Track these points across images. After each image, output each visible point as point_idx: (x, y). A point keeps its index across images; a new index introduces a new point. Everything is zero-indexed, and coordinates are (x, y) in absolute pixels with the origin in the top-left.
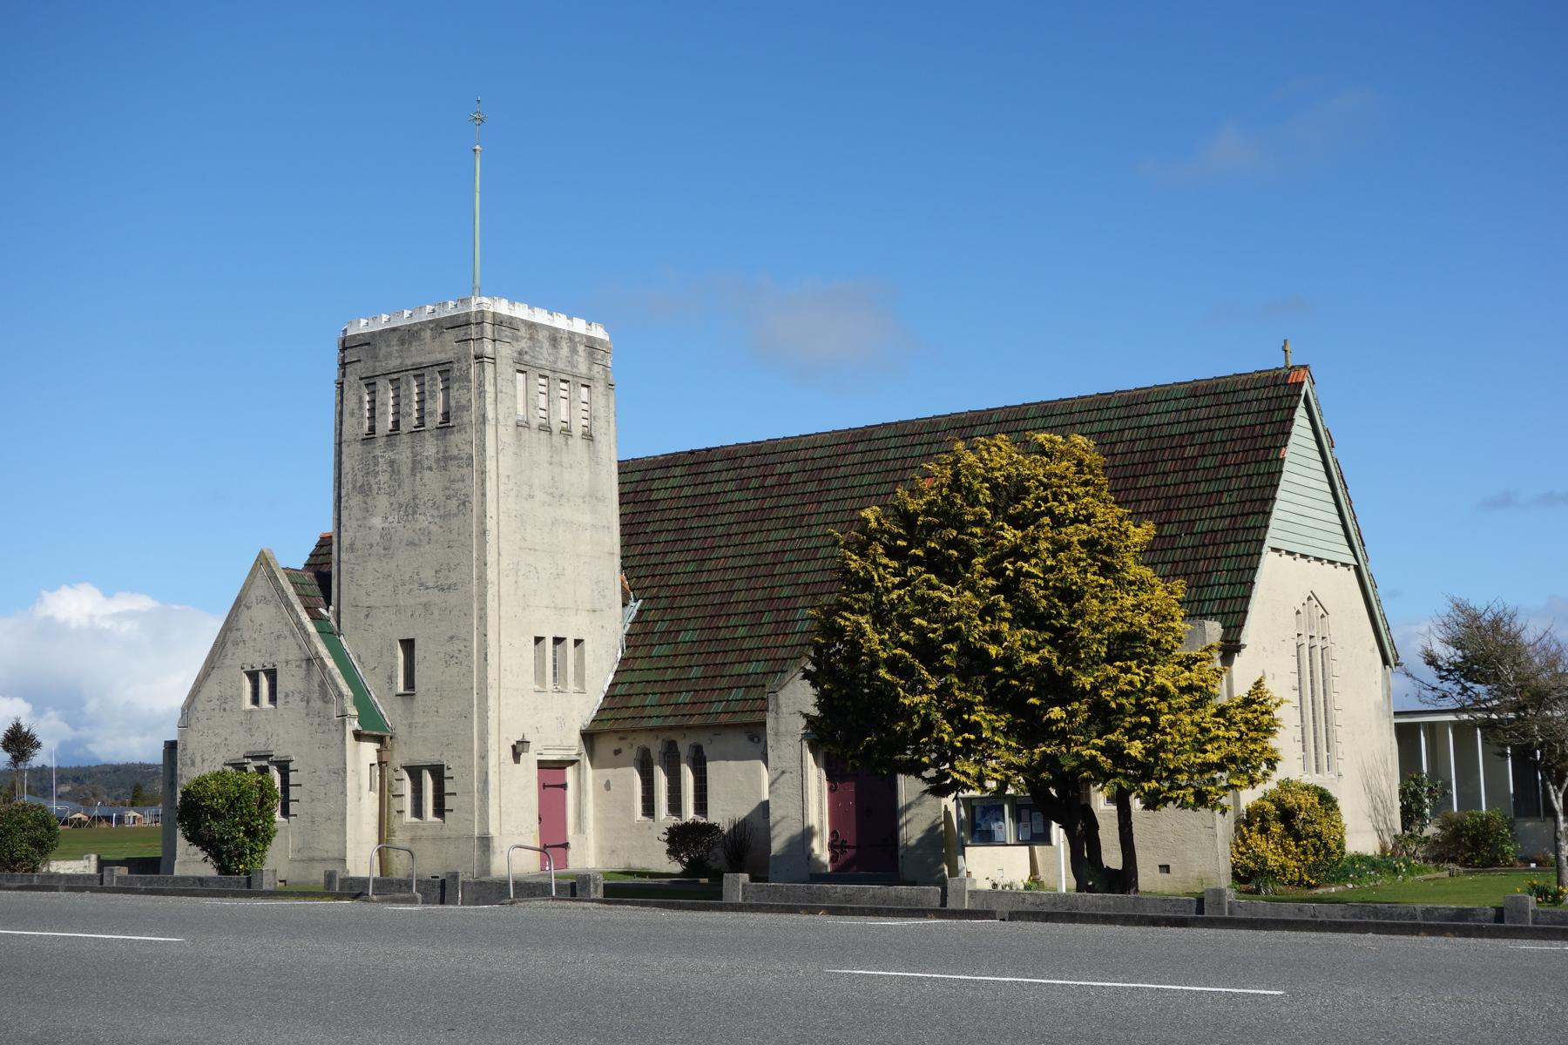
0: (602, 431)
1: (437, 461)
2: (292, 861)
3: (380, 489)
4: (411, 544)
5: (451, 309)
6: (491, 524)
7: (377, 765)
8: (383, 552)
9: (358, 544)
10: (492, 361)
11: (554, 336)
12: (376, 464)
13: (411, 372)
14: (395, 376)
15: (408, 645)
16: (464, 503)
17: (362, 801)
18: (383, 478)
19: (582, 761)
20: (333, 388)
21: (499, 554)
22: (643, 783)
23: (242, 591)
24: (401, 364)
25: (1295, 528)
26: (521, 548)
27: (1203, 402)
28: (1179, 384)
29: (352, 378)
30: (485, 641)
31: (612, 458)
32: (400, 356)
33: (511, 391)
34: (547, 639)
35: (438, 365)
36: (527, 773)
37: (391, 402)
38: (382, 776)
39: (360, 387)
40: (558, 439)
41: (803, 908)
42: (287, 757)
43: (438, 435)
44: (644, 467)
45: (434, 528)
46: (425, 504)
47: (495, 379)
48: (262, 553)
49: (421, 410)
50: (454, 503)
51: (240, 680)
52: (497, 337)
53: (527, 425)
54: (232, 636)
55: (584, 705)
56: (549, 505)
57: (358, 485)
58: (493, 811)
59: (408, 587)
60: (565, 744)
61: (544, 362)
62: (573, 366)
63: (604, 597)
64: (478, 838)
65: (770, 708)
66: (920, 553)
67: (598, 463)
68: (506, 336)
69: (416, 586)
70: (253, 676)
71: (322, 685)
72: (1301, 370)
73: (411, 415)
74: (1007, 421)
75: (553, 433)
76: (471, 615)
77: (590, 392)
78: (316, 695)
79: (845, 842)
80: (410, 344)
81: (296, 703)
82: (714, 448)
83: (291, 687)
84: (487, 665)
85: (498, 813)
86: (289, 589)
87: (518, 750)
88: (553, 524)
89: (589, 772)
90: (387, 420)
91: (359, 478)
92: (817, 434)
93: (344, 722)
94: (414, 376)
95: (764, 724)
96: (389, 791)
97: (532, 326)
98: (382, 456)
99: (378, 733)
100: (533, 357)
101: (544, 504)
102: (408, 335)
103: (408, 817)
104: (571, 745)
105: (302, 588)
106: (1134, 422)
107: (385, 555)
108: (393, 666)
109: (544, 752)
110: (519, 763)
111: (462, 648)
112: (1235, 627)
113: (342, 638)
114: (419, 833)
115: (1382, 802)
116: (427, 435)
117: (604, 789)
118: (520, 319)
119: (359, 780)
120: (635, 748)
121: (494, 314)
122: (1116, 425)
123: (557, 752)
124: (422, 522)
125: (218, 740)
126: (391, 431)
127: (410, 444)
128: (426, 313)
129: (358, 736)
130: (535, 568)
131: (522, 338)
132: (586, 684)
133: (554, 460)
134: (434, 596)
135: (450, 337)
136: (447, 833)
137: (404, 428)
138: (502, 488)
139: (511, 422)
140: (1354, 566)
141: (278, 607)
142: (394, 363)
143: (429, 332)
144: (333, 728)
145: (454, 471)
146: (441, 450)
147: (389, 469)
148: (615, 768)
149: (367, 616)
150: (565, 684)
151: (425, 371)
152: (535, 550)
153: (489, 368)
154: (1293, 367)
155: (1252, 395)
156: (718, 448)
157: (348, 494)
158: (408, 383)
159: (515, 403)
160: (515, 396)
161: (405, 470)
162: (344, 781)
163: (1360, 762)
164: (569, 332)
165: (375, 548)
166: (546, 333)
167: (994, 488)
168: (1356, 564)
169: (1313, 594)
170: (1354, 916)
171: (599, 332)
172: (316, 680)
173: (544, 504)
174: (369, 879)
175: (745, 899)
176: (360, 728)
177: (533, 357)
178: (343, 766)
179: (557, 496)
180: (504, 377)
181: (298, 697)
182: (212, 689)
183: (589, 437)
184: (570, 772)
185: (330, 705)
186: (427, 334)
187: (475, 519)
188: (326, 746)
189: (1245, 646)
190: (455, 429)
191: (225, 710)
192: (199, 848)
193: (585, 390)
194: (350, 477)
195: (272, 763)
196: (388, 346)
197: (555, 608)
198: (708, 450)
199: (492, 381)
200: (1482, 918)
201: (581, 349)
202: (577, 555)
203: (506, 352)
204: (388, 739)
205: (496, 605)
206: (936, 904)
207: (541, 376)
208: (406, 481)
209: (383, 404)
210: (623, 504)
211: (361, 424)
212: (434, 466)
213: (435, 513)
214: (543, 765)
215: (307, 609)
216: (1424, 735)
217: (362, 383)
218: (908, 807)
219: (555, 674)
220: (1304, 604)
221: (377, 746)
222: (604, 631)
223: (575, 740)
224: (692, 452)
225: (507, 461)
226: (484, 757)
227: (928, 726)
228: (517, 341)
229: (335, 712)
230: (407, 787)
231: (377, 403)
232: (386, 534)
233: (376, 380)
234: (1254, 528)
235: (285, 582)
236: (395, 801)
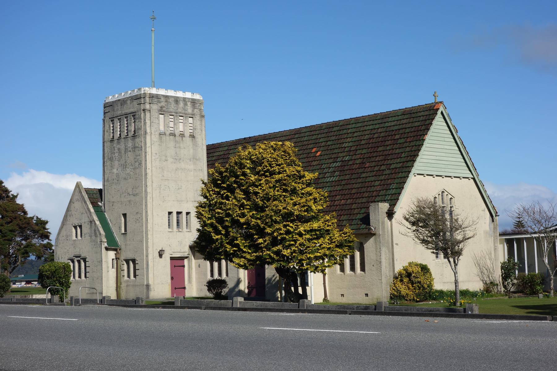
0: (199, 134)
1: (132, 148)
2: (88, 293)
3: (115, 159)
4: (125, 179)
5: (136, 92)
6: (149, 171)
7: (115, 259)
8: (117, 182)
9: (110, 179)
10: (149, 111)
11: (177, 100)
12: (114, 150)
13: (124, 116)
14: (119, 117)
15: (125, 215)
16: (140, 164)
18: (116, 155)
19: (190, 257)
20: (102, 122)
21: (152, 182)
23: (72, 197)
24: (121, 113)
25: (435, 166)
26: (162, 180)
27: (406, 116)
28: (400, 109)
29: (107, 118)
30: (147, 214)
31: (204, 143)
32: (121, 110)
33: (157, 122)
34: (174, 213)
35: (132, 113)
36: (166, 261)
37: (119, 127)
38: (117, 263)
39: (109, 121)
40: (178, 138)
41: (186, 307)
42: (85, 256)
43: (132, 139)
44: (229, 145)
45: (131, 173)
46: (129, 164)
47: (150, 118)
48: (77, 183)
49: (127, 130)
50: (137, 164)
51: (72, 229)
52: (151, 102)
53: (165, 134)
54: (69, 213)
55: (192, 236)
56: (175, 163)
57: (109, 157)
58: (151, 275)
59: (124, 195)
61: (172, 110)
62: (185, 110)
66: (225, 185)
67: (196, 146)
68: (155, 101)
69: (127, 194)
70: (75, 227)
71: (95, 231)
72: (440, 103)
73: (124, 131)
74: (344, 125)
76: (143, 205)
77: (193, 119)
78: (93, 234)
80: (124, 105)
81: (88, 237)
82: (252, 137)
83: (86, 232)
84: (148, 223)
85: (153, 276)
86: (86, 196)
87: (160, 253)
88: (176, 170)
90: (117, 134)
91: (110, 155)
92: (285, 131)
93: (101, 244)
94: (132, 116)
96: (120, 268)
97: (166, 97)
98: (116, 147)
99: (114, 248)
100: (167, 108)
101: (172, 163)
102: (123, 102)
103: (126, 278)
104: (185, 250)
105: (93, 195)
106: (382, 125)
107: (117, 183)
108: (121, 223)
109: (173, 254)
110: (162, 258)
111: (140, 217)
112: (393, 205)
113: (105, 213)
114: (129, 283)
115: (486, 269)
116: (129, 139)
121: (150, 94)
122: (377, 126)
123: (178, 254)
124: (128, 170)
125: (66, 251)
126: (119, 137)
127: (124, 142)
128: (129, 94)
129: (107, 249)
130: (168, 187)
131: (162, 102)
132: (192, 229)
134: (132, 198)
135: (135, 102)
136: (137, 283)
137: (122, 137)
138: (153, 158)
139: (157, 133)
140: (472, 178)
141: (82, 203)
142: (119, 113)
143: (129, 101)
144: (98, 246)
145: (137, 152)
146: (133, 144)
147: (118, 151)
149: (113, 205)
150: (173, 229)
151: (128, 115)
153: (148, 114)
154: (437, 102)
155: (422, 113)
156: (253, 137)
157: (106, 161)
158: (123, 120)
159: (159, 126)
160: (159, 124)
161: (123, 152)
162: (102, 265)
163: (473, 255)
164: (183, 98)
165: (115, 180)
166: (173, 99)
167: (253, 162)
168: (473, 177)
170: (339, 309)
171: (197, 97)
172: (93, 229)
173: (172, 163)
174: (46, 299)
175: (181, 305)
176: (107, 246)
178: (101, 260)
179: (178, 159)
180: (154, 117)
181: (88, 235)
182: (64, 233)
183: (192, 136)
184: (186, 261)
185: (97, 238)
186: (129, 102)
187: (143, 170)
188: (96, 253)
189: (395, 212)
190: (137, 137)
191: (67, 240)
193: (191, 119)
194: (107, 154)
195: (82, 259)
196: (117, 106)
198: (250, 138)
199: (149, 119)
200: (371, 309)
201: (189, 104)
202: (187, 181)
203: (155, 107)
204: (118, 250)
205: (151, 200)
206: (231, 306)
207: (170, 115)
208: (123, 156)
209: (116, 128)
211: (110, 135)
212: (131, 150)
213: (132, 167)
214: (172, 259)
215: (92, 203)
216: (526, 242)
217: (110, 120)
219: (187, 225)
220: (439, 194)
221: (115, 252)
223: (187, 249)
224: (245, 139)
225: (155, 148)
226: (147, 256)
227: (222, 245)
228: (160, 103)
229: (99, 241)
230: (125, 267)
231: (114, 127)
232: (118, 175)
233: (114, 119)
234: (409, 167)
235: (84, 194)
236: (122, 272)
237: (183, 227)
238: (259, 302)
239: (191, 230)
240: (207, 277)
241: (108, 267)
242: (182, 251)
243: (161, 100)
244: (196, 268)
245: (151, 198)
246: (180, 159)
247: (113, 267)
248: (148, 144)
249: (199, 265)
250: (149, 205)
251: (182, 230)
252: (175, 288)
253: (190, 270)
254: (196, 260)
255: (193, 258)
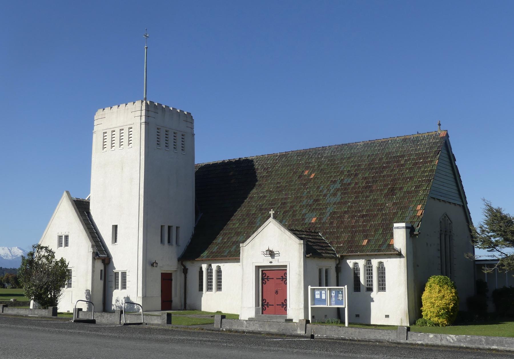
79: (281, 280)
140: (462, 206)
168: (463, 205)
169: (447, 215)
210: (213, 323)
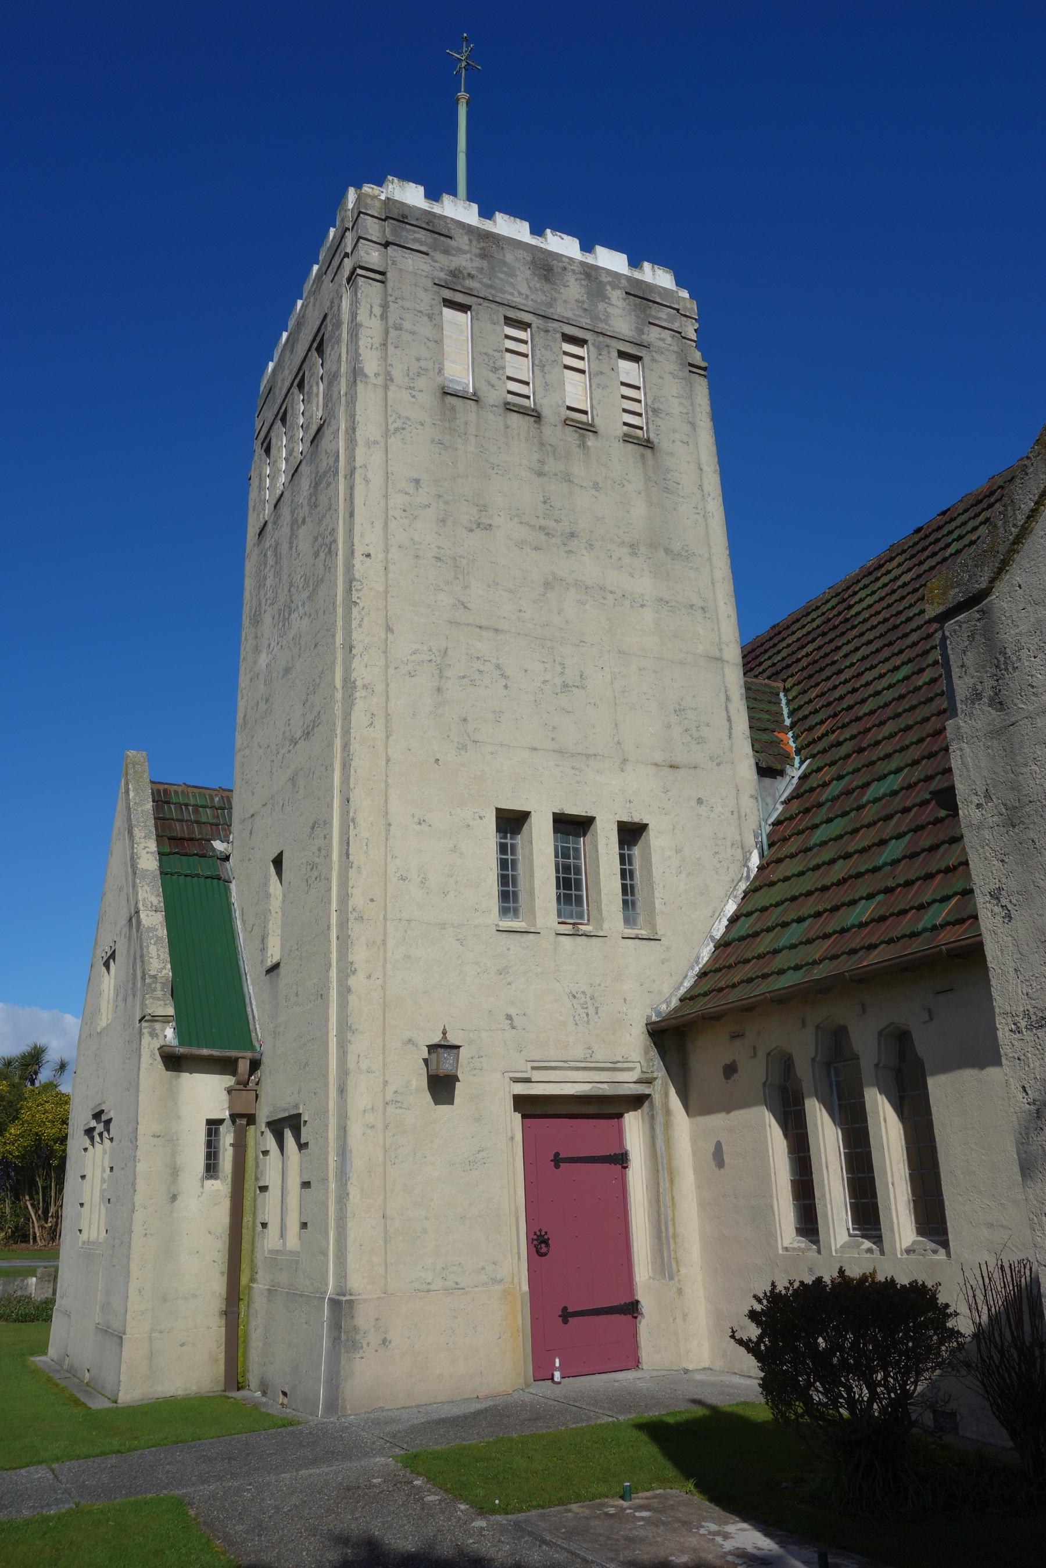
0: (677, 436)
7: (228, 1122)
17: (180, 1202)
19: (657, 1098)
22: (791, 1151)
34: (534, 819)
38: (240, 1147)
40: (554, 433)
47: (385, 306)
52: (391, 239)
56: (536, 548)
60: (599, 1056)
63: (701, 741)
64: (331, 1300)
65: (962, 687)
75: (544, 420)
89: (682, 1122)
95: (952, 788)
99: (215, 1053)
101: (520, 544)
109: (536, 1076)
117: (712, 1164)
118: (452, 219)
119: (174, 1154)
120: (762, 1054)
129: (173, 1062)
130: (498, 667)
132: (659, 920)
133: (546, 468)
148: (728, 1112)
152: (496, 630)
173: (520, 544)
177: (490, 287)
184: (633, 1124)
192: (880, 1278)
197: (560, 752)
199: (378, 311)
204: (243, 1066)
218: (756, 1378)
221: (229, 1081)
222: (703, 809)
237: (600, 911)
238: (337, 669)
239: (653, 926)
240: (770, 1236)
241: (175, 1172)
242: (602, 1055)
243: (452, 243)
244: (697, 1170)
245: (380, 723)
246: (572, 535)
247: (211, 1169)
248: (369, 427)
249: (719, 1146)
250: (361, 764)
251: (600, 921)
252: (566, 1315)
253: (664, 1185)
254: (717, 1120)
255: (675, 1102)
